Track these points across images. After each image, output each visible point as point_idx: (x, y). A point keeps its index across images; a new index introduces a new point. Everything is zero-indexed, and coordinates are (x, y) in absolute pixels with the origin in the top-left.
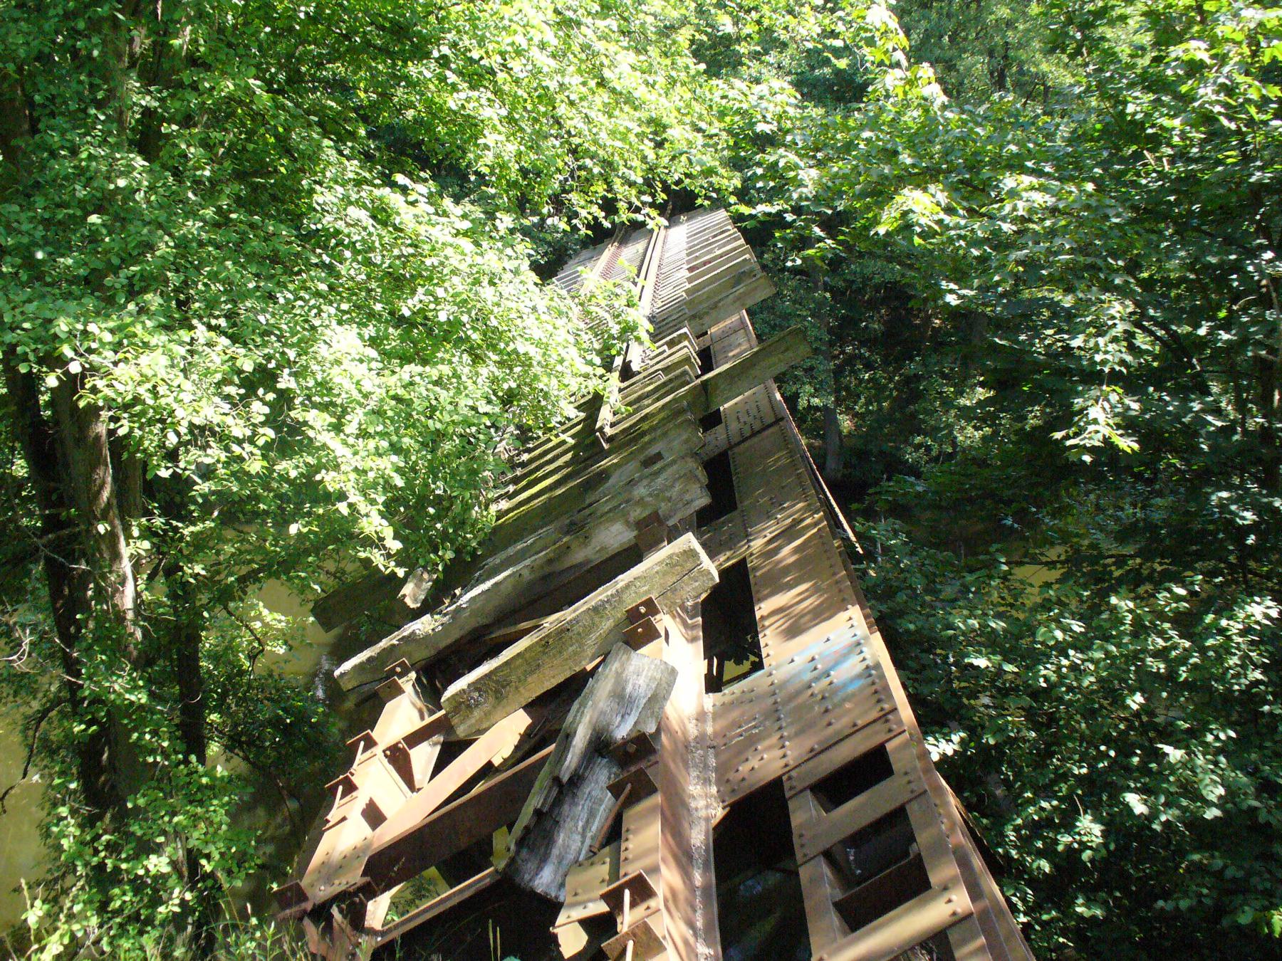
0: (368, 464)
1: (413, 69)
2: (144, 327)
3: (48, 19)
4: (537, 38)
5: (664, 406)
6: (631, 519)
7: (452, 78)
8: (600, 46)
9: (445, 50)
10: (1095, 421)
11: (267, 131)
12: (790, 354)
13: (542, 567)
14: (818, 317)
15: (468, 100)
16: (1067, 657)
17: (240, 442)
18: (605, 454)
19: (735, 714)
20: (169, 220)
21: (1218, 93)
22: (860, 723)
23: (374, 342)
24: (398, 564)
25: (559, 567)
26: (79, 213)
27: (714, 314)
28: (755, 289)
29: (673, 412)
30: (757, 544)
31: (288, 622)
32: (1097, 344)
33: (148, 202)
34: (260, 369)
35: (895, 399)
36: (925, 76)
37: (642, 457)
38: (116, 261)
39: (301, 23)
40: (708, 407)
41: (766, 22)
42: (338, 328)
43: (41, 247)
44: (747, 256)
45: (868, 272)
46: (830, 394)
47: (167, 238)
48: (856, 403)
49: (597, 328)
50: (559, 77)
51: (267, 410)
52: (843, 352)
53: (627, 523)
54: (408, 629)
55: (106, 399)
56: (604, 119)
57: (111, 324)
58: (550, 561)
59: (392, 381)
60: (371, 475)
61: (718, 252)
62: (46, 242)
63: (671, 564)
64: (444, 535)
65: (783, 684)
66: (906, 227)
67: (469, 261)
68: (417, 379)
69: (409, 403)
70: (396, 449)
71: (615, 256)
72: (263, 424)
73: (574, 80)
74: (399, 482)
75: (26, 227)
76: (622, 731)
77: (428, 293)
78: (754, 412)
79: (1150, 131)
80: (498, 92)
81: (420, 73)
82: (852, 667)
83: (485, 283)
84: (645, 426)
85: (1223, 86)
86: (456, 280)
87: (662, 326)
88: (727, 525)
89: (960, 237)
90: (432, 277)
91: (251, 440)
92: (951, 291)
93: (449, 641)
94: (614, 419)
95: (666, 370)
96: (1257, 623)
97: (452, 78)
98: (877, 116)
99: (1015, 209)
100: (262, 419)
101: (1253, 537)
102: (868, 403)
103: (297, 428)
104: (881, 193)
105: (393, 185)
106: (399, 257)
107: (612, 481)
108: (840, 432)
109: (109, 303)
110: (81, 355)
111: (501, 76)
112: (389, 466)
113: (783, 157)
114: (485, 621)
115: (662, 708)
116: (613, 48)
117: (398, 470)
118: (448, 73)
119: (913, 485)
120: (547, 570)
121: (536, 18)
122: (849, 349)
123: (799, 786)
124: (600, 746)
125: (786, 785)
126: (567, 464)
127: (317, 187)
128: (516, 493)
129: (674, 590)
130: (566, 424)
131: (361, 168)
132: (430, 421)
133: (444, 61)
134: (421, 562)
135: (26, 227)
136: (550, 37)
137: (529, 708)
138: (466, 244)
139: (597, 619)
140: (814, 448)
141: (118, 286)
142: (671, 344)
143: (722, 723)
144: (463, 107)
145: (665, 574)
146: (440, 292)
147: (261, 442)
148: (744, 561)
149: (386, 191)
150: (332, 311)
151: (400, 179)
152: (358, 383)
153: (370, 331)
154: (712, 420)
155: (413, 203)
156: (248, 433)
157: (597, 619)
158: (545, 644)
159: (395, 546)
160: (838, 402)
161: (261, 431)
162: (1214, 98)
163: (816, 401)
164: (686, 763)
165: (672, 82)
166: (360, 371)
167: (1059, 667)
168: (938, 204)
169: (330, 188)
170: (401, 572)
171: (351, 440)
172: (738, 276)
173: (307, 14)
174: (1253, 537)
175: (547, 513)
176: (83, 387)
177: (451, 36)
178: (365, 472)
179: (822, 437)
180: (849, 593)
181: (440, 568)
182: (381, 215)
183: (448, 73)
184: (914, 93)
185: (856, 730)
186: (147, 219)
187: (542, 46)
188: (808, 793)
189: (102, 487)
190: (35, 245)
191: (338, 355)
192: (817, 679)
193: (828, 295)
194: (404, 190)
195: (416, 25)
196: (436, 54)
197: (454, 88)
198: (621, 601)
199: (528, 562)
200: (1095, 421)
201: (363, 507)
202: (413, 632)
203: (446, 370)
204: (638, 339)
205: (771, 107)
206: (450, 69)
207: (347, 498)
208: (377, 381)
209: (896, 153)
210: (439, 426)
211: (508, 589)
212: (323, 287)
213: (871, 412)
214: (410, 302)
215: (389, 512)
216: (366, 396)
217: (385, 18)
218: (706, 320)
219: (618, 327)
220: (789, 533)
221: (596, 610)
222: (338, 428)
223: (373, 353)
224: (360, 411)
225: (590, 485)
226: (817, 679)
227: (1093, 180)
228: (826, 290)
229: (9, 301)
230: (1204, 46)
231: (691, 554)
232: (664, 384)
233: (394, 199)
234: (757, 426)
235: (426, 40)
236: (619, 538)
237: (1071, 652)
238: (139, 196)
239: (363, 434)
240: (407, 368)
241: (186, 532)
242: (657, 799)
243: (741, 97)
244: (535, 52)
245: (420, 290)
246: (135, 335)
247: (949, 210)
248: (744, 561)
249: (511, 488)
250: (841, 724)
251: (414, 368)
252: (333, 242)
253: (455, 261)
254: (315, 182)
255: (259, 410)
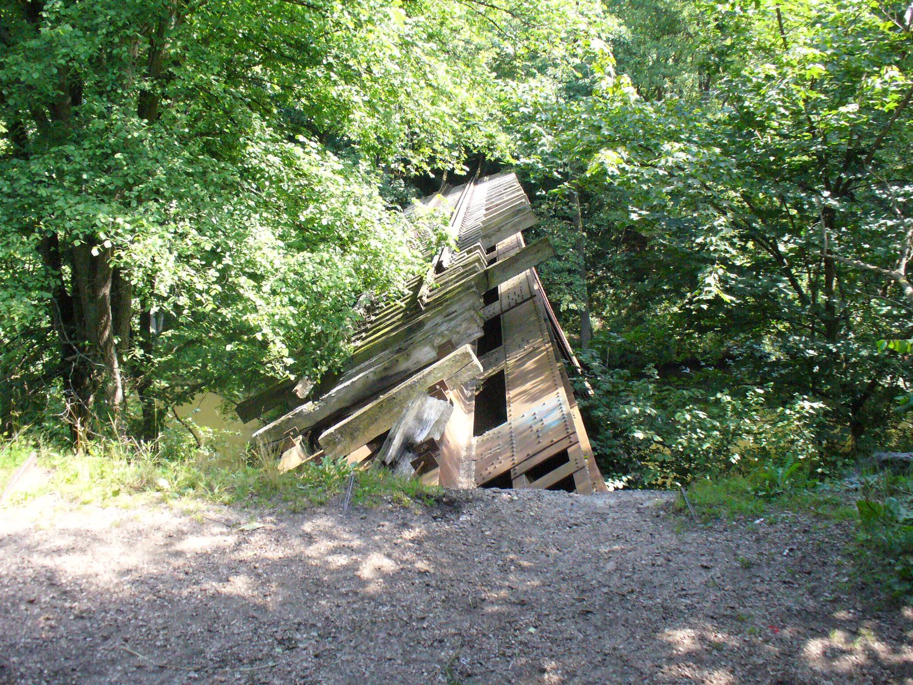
0: (276, 311)
1: (309, 71)
2: (148, 220)
3: (98, 36)
4: (388, 53)
5: (460, 286)
6: (435, 345)
7: (334, 77)
8: (426, 59)
9: (331, 60)
10: (709, 285)
11: (219, 107)
12: (539, 255)
13: (381, 372)
14: (578, 250)
15: (343, 90)
16: (696, 433)
17: (201, 293)
18: (421, 312)
19: (488, 445)
20: (163, 158)
21: (778, 94)
22: (555, 440)
23: (282, 237)
24: (291, 373)
25: (390, 373)
26: (109, 151)
27: (499, 234)
28: (525, 219)
29: (467, 288)
30: (511, 362)
31: (214, 433)
32: (711, 241)
33: (151, 146)
34: (213, 251)
35: (630, 308)
36: (626, 82)
37: (444, 314)
38: (131, 181)
39: (240, 40)
40: (488, 286)
41: (532, 48)
42: (261, 229)
43: (87, 172)
44: (523, 200)
45: (611, 218)
46: (583, 301)
47: (161, 168)
48: (603, 310)
49: (421, 236)
50: (400, 78)
51: (217, 274)
52: (596, 275)
53: (433, 347)
54: (298, 409)
55: (126, 263)
56: (428, 105)
57: (128, 219)
58: (386, 369)
59: (292, 261)
60: (277, 318)
61: (506, 199)
62: (91, 168)
63: (455, 361)
64: (322, 357)
65: (517, 428)
66: (604, 173)
67: (342, 190)
68: (307, 260)
69: (302, 275)
70: (293, 303)
71: (439, 202)
72: (214, 283)
73: (410, 79)
74: (292, 323)
75: (78, 159)
76: (420, 438)
77: (315, 207)
78: (518, 292)
79: (758, 119)
80: (363, 87)
81: (315, 73)
82: (557, 415)
83: (351, 202)
84: (448, 296)
85: (783, 90)
86: (333, 200)
87: (464, 243)
88: (496, 353)
89: (634, 178)
90: (318, 198)
91: (207, 292)
92: (634, 212)
93: (322, 418)
94: (430, 294)
95: (463, 267)
96: (807, 412)
97: (334, 77)
98: (593, 106)
99: (667, 162)
100: (214, 279)
101: (817, 367)
102: (612, 309)
103: (233, 287)
104: (588, 152)
105: (297, 142)
106: (298, 186)
107: (425, 328)
108: (591, 330)
109: (126, 205)
110: (112, 237)
111: (365, 76)
112: (288, 313)
113: (534, 128)
114: (344, 405)
115: (444, 427)
116: (433, 60)
117: (293, 315)
118: (332, 74)
119: (616, 338)
120: (384, 374)
121: (387, 42)
122: (599, 273)
123: (519, 473)
124: (408, 446)
125: (512, 473)
126: (399, 320)
127: (249, 142)
128: (366, 337)
129: (456, 376)
130: (400, 296)
131: (275, 132)
132: (314, 286)
133: (329, 66)
134: (307, 373)
135: (78, 159)
136: (396, 52)
137: (369, 444)
138: (340, 178)
139: (411, 392)
140: (573, 339)
141: (133, 196)
142: (469, 252)
143: (479, 451)
144: (340, 95)
145: (452, 366)
146: (323, 207)
147: (213, 293)
148: (502, 371)
149: (291, 146)
150: (257, 216)
151: (301, 138)
152: (271, 262)
153: (279, 231)
154: (491, 296)
155: (308, 153)
156: (206, 287)
157: (411, 392)
158: (381, 406)
159: (290, 361)
160: (591, 308)
161: (214, 286)
162: (777, 97)
163: (573, 306)
164: (458, 468)
165: (474, 83)
166: (272, 255)
167: (690, 438)
168: (622, 158)
169: (257, 143)
170: (292, 377)
171: (266, 296)
172: (517, 211)
173: (243, 34)
174: (817, 367)
175: (384, 346)
176: (112, 255)
177: (335, 51)
178: (273, 315)
179: (579, 333)
180: (559, 380)
181: (319, 376)
182: (288, 160)
183: (332, 74)
184: (618, 92)
185: (553, 444)
186: (151, 157)
187: (392, 58)
188: (524, 476)
189: (105, 328)
190: (82, 170)
191: (260, 244)
192: (536, 423)
193: (585, 234)
194: (303, 145)
195: (311, 43)
196: (325, 62)
197: (335, 83)
198: (425, 382)
199: (372, 369)
200: (709, 285)
201: (271, 336)
202: (302, 411)
203: (326, 256)
204: (448, 245)
205: (529, 98)
206: (333, 71)
207: (261, 330)
208: (283, 261)
209: (600, 128)
210: (320, 289)
211: (359, 386)
212: (252, 203)
213: (613, 316)
214: (305, 212)
215: (289, 341)
216: (276, 270)
217: (292, 39)
218: (493, 239)
219: (435, 237)
220: (530, 355)
221: (411, 386)
222: (259, 288)
223: (282, 244)
224: (272, 279)
225: (411, 331)
226: (536, 423)
227: (720, 145)
228: (584, 231)
229: (67, 203)
230: (773, 67)
231: (467, 355)
232: (462, 273)
233: (298, 151)
234: (519, 300)
235: (318, 53)
236: (428, 355)
237: (699, 430)
238: (146, 143)
239: (274, 292)
240: (301, 254)
241: (155, 361)
242: (438, 470)
243: (512, 91)
244: (386, 61)
245: (311, 206)
246: (143, 226)
247: (628, 162)
248: (502, 371)
249: (364, 335)
250: (545, 442)
251: (306, 254)
252: (258, 176)
253: (332, 189)
254: (248, 139)
255: (213, 274)
